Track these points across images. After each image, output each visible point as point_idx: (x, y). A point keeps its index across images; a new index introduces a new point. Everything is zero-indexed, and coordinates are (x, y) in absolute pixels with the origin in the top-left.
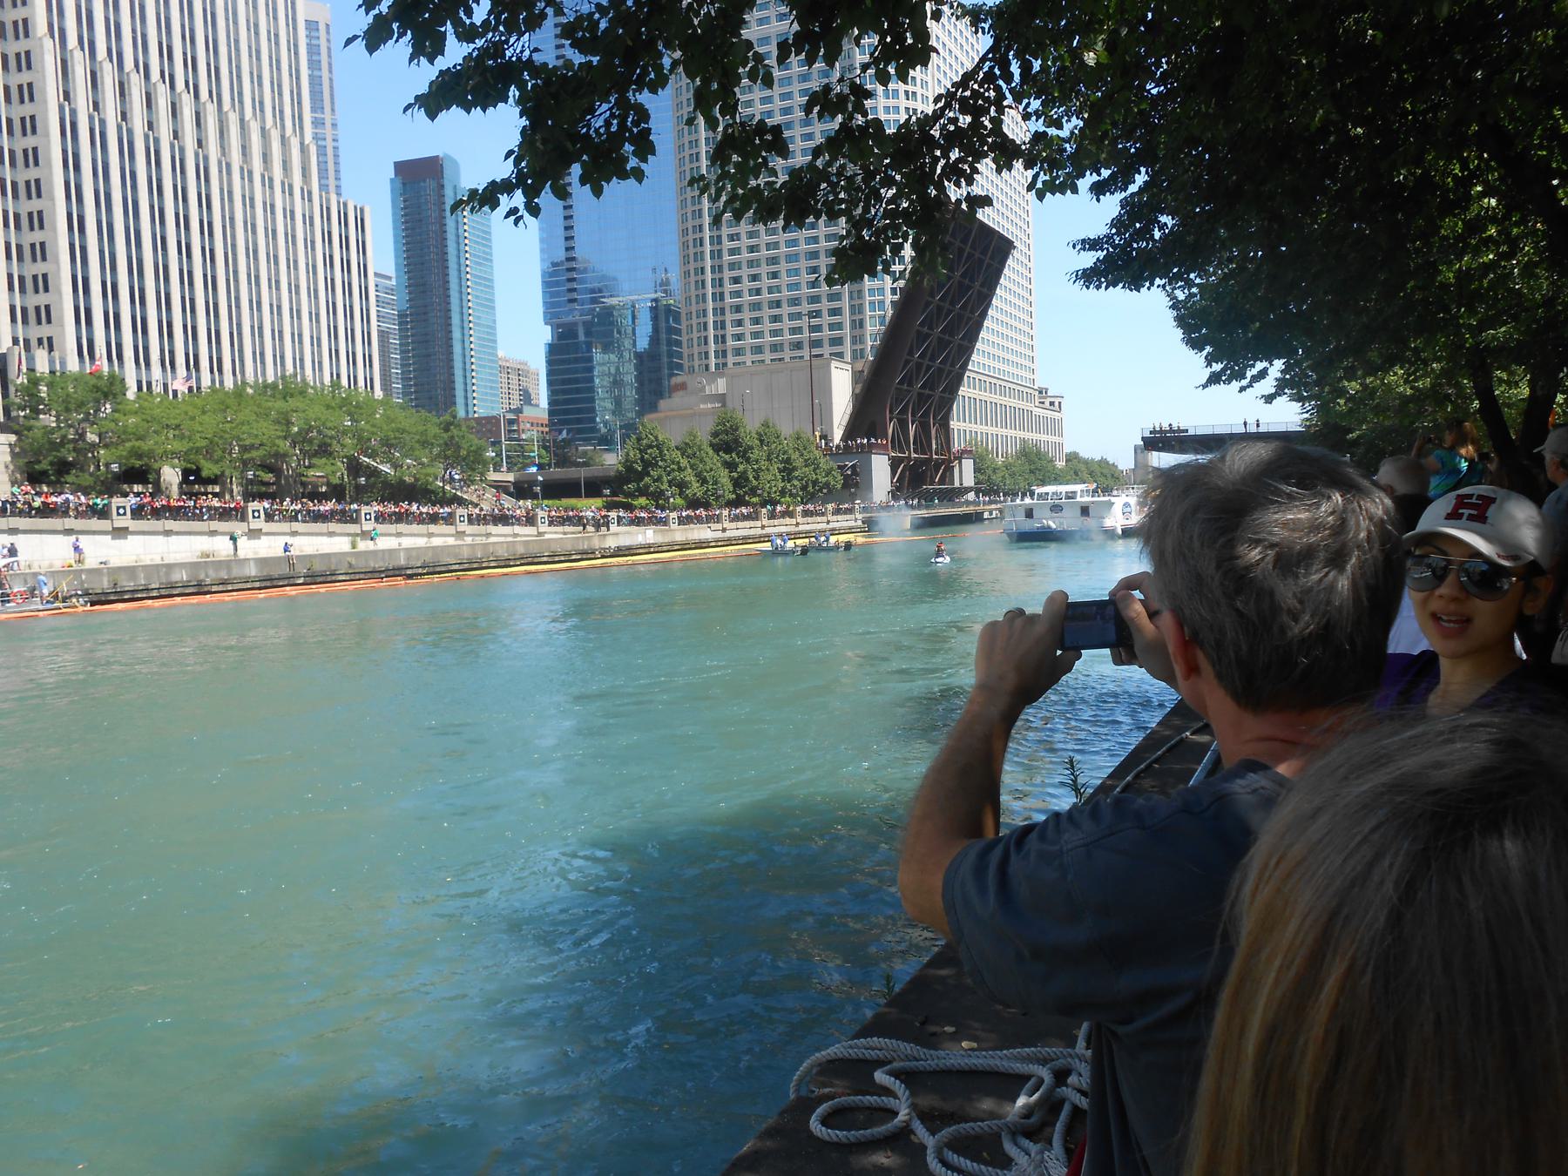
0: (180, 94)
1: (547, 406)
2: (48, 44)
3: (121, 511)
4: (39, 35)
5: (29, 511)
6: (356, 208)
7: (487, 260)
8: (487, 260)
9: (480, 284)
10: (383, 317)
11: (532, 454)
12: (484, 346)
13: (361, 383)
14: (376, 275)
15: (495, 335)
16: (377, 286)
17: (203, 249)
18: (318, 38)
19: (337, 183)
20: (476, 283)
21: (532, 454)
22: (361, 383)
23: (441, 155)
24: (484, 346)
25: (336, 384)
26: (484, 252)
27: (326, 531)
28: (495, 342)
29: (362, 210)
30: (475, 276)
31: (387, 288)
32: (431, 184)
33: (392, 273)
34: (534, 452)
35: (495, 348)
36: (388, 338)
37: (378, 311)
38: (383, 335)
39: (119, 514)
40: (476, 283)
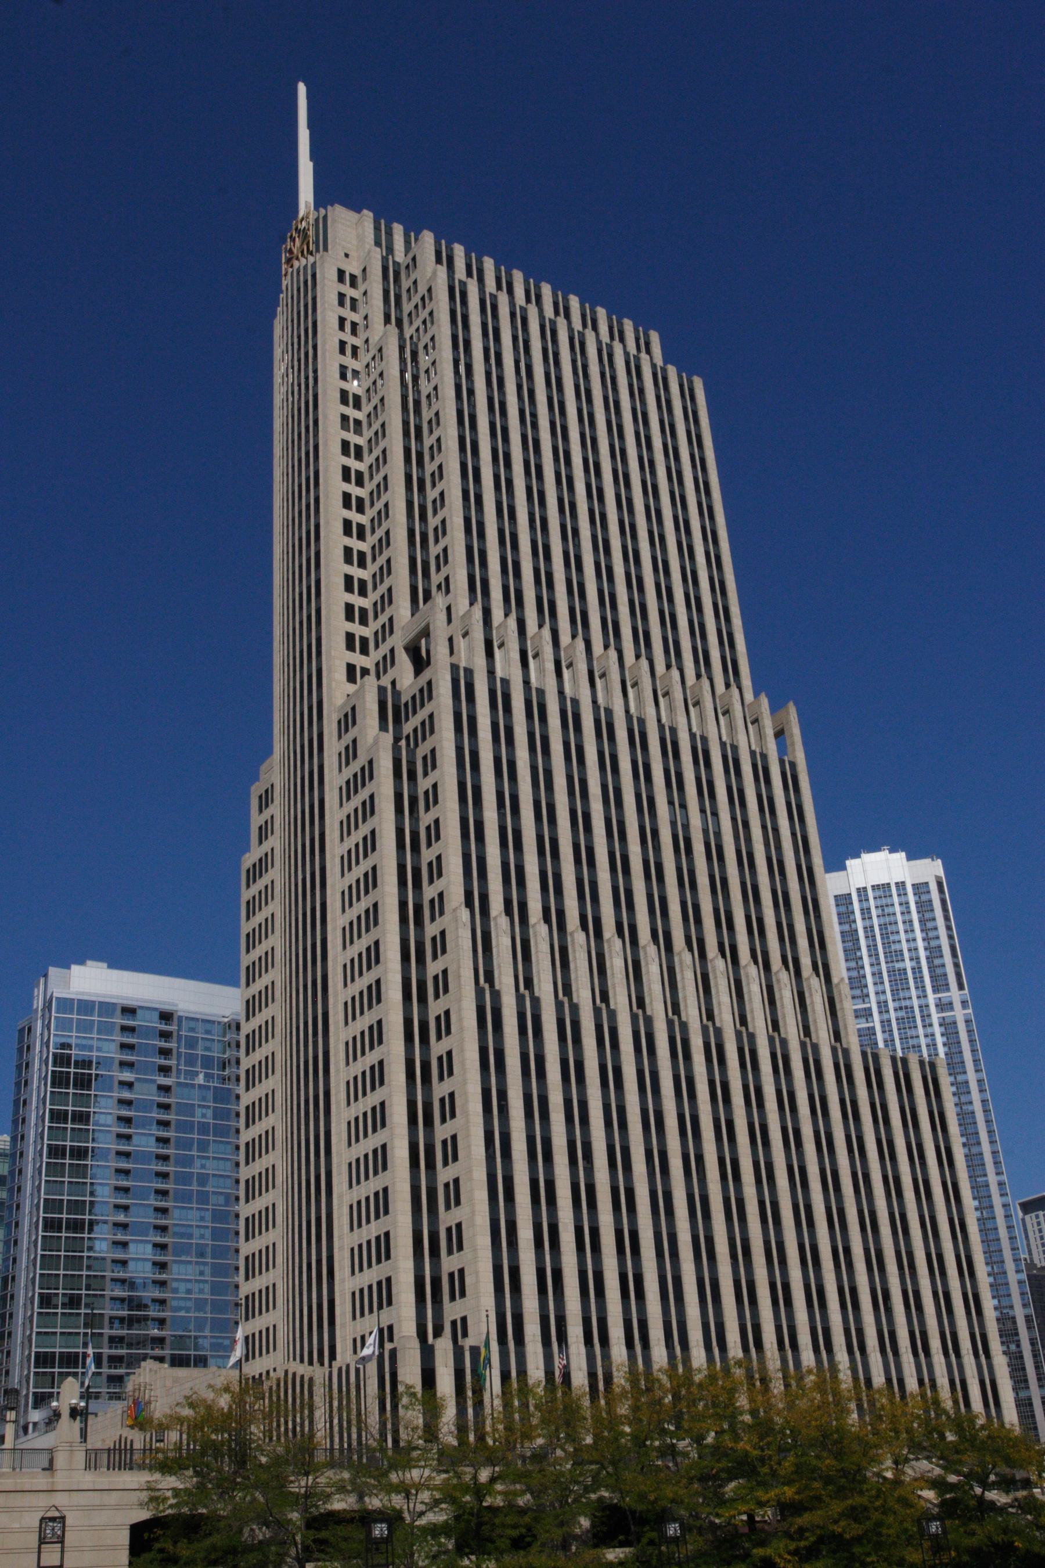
13: (942, 1381)
22: (942, 1381)
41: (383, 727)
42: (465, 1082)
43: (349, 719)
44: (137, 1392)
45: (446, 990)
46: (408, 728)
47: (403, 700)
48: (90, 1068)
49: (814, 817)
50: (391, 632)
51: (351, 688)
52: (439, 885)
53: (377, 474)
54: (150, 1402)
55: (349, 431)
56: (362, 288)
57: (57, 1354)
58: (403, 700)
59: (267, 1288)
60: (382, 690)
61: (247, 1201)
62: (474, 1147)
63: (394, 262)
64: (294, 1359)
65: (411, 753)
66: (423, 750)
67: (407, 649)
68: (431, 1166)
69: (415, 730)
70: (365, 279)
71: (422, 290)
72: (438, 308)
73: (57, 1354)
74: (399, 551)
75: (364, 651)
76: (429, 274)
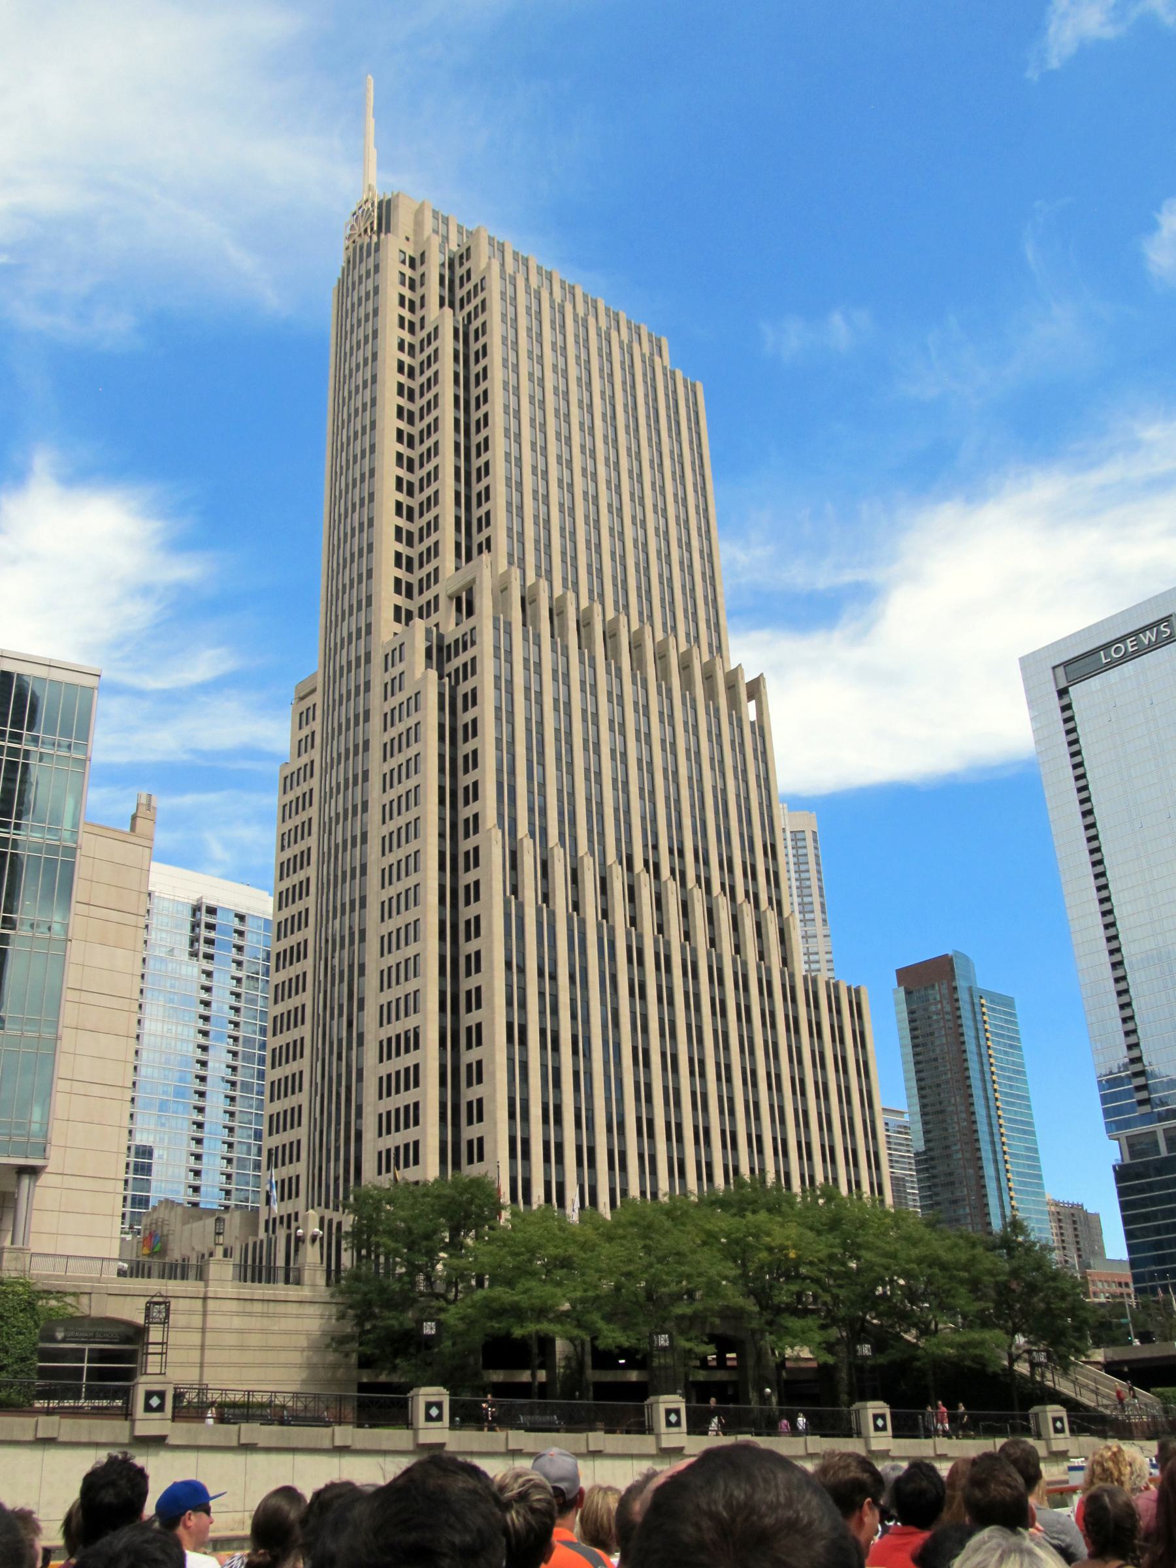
0: (639, 874)
1: (1124, 1255)
2: (497, 834)
3: (155, 1402)
4: (488, 827)
5: (93, 1414)
6: (849, 989)
7: (1018, 1072)
8: (1018, 1072)
9: (1013, 1104)
10: (897, 1162)
11: (1123, 1321)
12: (1025, 1184)
13: (866, 1187)
14: (884, 1110)
15: (1039, 1168)
16: (886, 1124)
17: (663, 1055)
18: (804, 839)
19: (881, 1197)
20: (1007, 1103)
21: (1123, 1321)
22: (866, 1187)
23: (950, 953)
24: (1025, 1184)
25: (830, 1193)
26: (1014, 1063)
27: (327, 1444)
28: (1040, 1177)
29: (857, 991)
30: (1006, 1094)
31: (900, 1126)
32: (937, 993)
33: (903, 1107)
34: (1125, 1316)
35: (1041, 1186)
36: (904, 1186)
37: (890, 1155)
38: (897, 1182)
39: (429, 1418)
40: (1007, 1103)
41: (428, 665)
42: (492, 978)
43: (397, 654)
44: (154, 1226)
45: (477, 898)
46: (450, 667)
47: (446, 643)
48: (136, 1164)
49: (772, 951)
50: (436, 582)
51: (399, 628)
52: (473, 808)
53: (428, 438)
54: (167, 1236)
55: (407, 582)
56: (420, 270)
57: (7, 739)
58: (446, 643)
59: (293, 1109)
60: (428, 631)
61: (274, 1034)
62: (495, 924)
63: (450, 250)
64: (319, 1205)
65: (453, 690)
66: (464, 688)
67: (450, 598)
68: (454, 906)
69: (457, 670)
70: (422, 263)
71: (475, 279)
72: (491, 296)
73: (7, 739)
74: (447, 511)
75: (409, 595)
76: (483, 265)
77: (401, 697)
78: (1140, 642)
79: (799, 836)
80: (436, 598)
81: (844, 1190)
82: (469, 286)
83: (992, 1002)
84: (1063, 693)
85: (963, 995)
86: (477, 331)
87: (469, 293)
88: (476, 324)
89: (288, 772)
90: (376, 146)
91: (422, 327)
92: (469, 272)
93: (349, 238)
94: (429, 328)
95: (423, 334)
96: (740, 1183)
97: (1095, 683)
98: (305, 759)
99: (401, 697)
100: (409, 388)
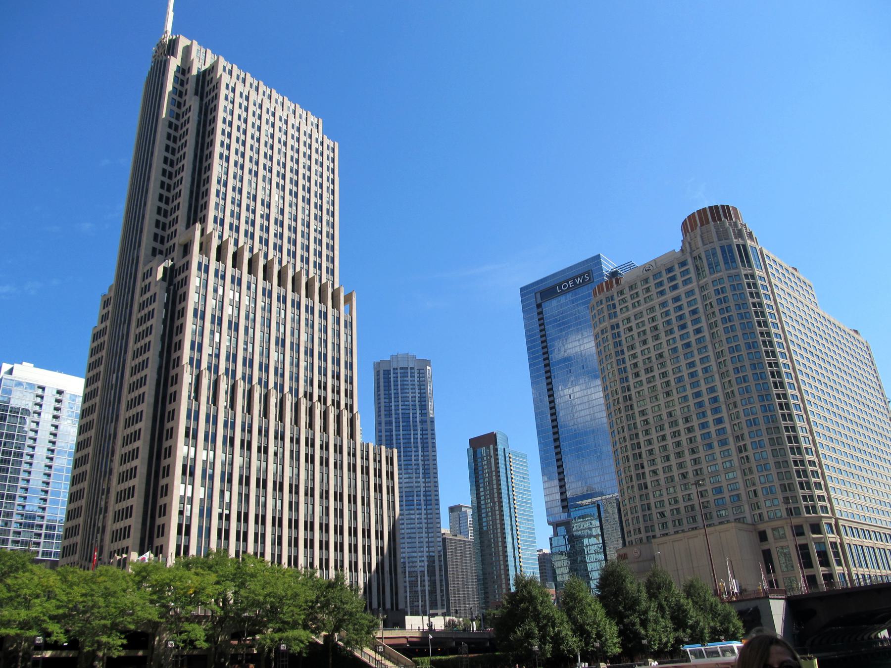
13: (285, 560)
22: (285, 560)
30: (519, 501)
77: (148, 295)
78: (575, 283)
79: (421, 371)
80: (174, 245)
81: (268, 557)
82: (211, 86)
83: (515, 456)
84: (539, 306)
85: (500, 453)
86: (212, 109)
87: (210, 90)
88: (212, 105)
89: (95, 331)
90: (174, 10)
91: (184, 105)
92: (212, 79)
93: (154, 57)
94: (187, 106)
95: (184, 109)
96: (208, 554)
97: (554, 303)
98: (103, 325)
99: (148, 295)
100: (174, 136)
